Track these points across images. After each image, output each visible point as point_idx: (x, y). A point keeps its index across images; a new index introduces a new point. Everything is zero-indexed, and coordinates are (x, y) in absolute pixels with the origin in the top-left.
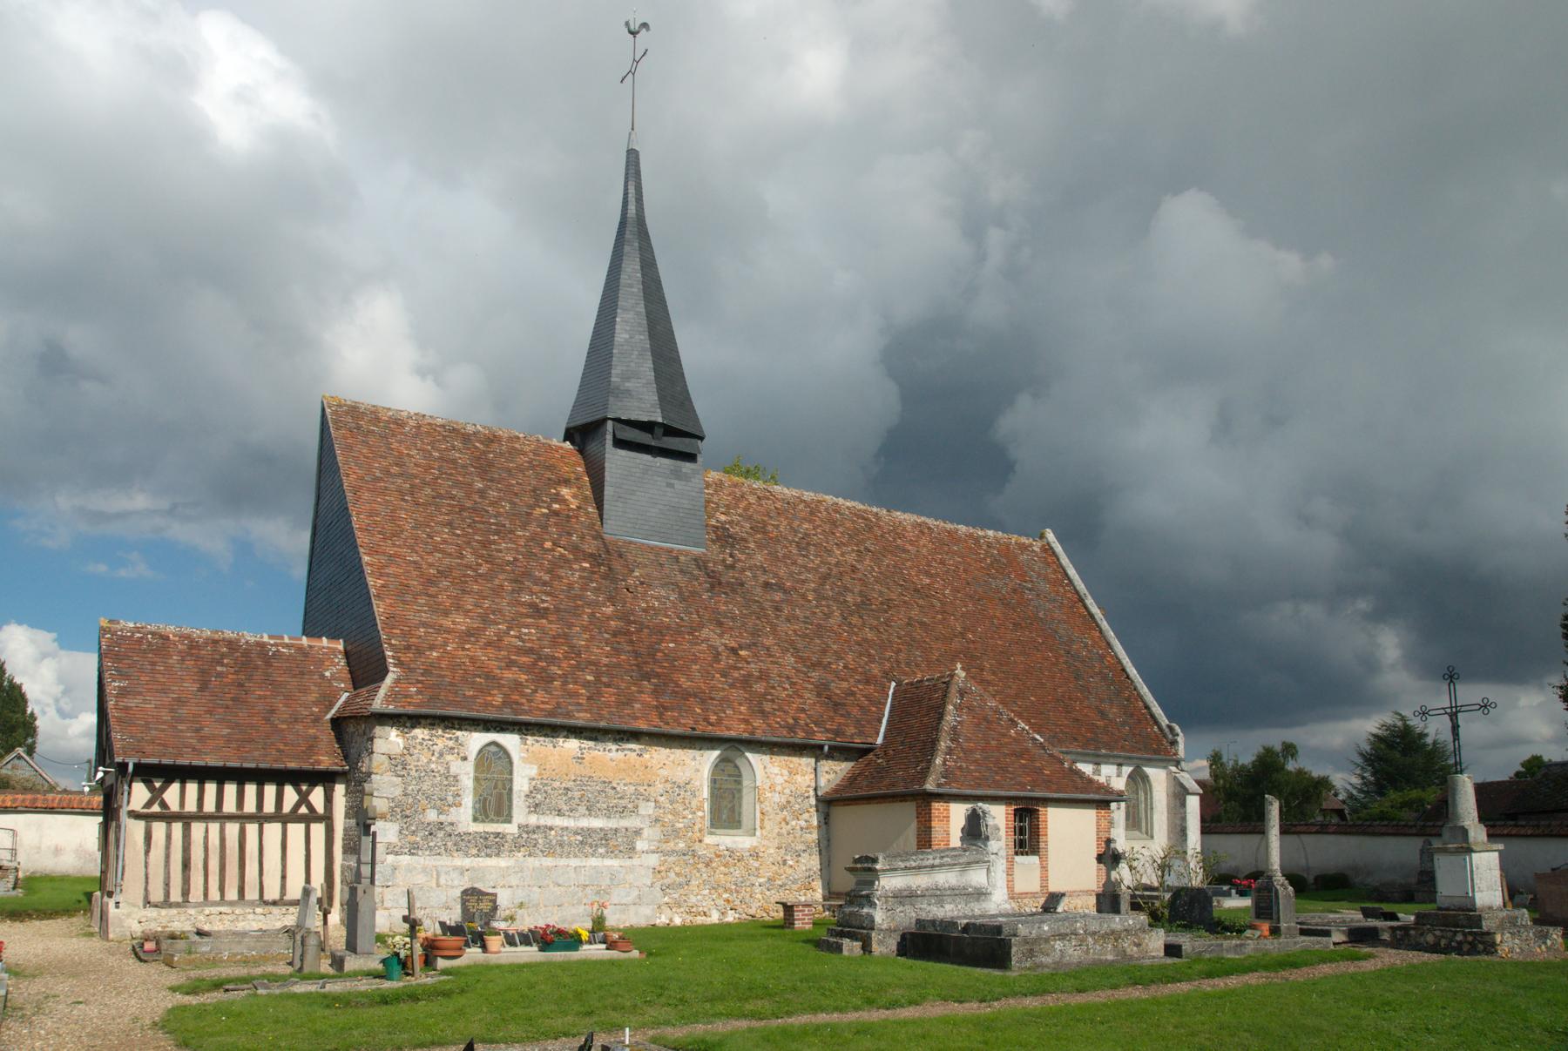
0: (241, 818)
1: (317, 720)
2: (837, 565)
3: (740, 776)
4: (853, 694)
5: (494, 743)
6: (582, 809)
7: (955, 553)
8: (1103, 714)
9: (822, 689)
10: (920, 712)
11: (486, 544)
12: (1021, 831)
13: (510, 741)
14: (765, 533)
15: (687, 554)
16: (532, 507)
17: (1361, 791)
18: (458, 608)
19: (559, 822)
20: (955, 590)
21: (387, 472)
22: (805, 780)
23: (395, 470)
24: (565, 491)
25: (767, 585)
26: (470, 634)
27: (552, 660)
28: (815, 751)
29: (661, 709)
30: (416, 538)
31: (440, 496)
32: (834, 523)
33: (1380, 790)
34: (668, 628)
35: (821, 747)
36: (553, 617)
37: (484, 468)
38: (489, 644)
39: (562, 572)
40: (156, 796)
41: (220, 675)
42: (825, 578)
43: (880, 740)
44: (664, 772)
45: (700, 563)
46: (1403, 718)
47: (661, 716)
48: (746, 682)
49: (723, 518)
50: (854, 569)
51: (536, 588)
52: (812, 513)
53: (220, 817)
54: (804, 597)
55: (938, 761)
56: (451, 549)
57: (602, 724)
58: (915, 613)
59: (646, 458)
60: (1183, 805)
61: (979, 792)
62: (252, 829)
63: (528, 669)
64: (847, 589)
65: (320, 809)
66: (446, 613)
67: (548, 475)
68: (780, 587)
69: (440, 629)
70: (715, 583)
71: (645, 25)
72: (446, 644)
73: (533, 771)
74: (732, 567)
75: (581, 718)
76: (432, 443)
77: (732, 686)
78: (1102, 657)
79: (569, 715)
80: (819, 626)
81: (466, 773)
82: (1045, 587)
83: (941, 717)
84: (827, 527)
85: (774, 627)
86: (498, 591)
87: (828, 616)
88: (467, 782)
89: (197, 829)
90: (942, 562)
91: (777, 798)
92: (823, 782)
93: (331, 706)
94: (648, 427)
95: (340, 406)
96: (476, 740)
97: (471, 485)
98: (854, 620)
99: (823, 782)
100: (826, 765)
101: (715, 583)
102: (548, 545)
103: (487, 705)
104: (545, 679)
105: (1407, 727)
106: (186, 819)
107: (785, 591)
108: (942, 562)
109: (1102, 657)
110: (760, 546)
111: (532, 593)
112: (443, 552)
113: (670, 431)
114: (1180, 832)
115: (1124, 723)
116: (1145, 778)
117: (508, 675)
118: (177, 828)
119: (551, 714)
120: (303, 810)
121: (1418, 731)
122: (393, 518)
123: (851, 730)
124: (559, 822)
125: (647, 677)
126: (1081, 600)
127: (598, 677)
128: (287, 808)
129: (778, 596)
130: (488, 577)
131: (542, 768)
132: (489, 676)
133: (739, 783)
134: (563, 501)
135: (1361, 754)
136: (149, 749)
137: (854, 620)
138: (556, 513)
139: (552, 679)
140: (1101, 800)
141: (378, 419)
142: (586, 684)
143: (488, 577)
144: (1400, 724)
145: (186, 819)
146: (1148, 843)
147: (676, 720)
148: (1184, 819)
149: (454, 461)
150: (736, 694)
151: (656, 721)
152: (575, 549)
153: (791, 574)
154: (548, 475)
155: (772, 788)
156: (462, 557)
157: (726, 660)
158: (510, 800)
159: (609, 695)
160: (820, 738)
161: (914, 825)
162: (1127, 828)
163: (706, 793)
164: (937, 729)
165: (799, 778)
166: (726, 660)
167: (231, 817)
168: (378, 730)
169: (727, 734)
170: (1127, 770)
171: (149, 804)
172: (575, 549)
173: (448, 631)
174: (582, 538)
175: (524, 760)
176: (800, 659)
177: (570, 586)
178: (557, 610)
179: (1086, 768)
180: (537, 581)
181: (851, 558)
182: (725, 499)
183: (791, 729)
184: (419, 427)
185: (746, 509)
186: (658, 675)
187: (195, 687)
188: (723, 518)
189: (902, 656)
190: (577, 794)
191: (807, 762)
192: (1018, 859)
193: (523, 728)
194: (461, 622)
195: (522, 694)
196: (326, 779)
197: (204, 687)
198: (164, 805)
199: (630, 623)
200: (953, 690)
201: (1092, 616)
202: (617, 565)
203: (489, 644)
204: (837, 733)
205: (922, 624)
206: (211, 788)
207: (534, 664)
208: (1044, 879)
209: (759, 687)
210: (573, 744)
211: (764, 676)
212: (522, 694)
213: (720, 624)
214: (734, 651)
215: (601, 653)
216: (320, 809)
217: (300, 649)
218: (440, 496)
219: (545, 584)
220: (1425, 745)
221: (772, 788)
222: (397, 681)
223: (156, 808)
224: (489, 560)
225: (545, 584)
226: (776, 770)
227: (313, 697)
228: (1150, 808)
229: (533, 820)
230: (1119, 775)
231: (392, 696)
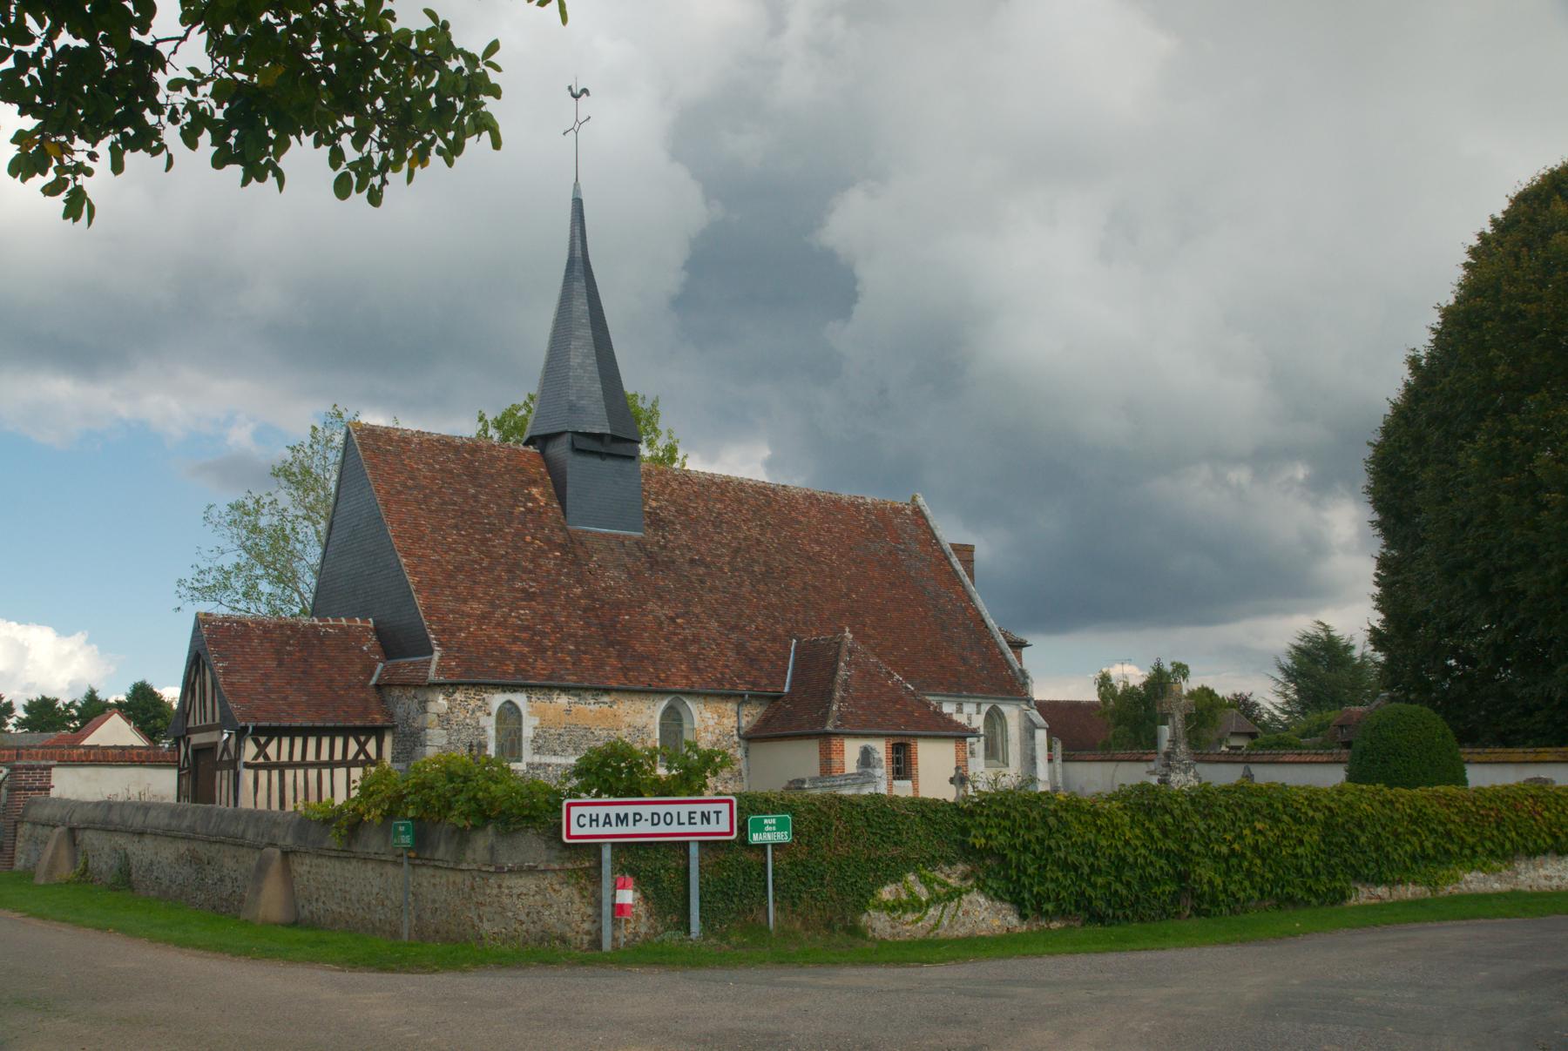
0: (319, 765)
1: (364, 686)
2: (745, 539)
3: (681, 720)
4: (764, 651)
5: (509, 702)
6: (570, 750)
7: (840, 521)
8: (964, 660)
9: (740, 648)
10: (817, 665)
11: (484, 541)
12: (898, 761)
13: (520, 699)
14: (687, 515)
15: (630, 538)
16: (513, 506)
17: (1283, 711)
18: (474, 597)
19: (554, 760)
20: (841, 556)
21: (404, 485)
22: (730, 722)
23: (410, 483)
24: (534, 491)
25: (692, 561)
26: (484, 617)
27: (543, 634)
28: (740, 699)
29: (625, 671)
30: (435, 540)
31: (445, 503)
32: (740, 501)
33: (49, 768)
34: (623, 603)
35: (742, 696)
36: (540, 600)
37: (474, 476)
38: (499, 624)
39: (542, 561)
40: (262, 749)
41: (289, 653)
42: (737, 551)
43: (786, 689)
44: (627, 719)
45: (640, 544)
46: (1326, 629)
47: (625, 675)
48: (683, 644)
49: (654, 504)
50: (758, 542)
51: (525, 576)
52: (722, 494)
53: (304, 764)
54: (721, 569)
55: (835, 708)
56: (460, 548)
57: (586, 684)
58: (809, 578)
59: (596, 461)
60: (1033, 737)
61: (866, 731)
62: (326, 773)
63: (528, 643)
64: (754, 561)
65: (373, 755)
66: (465, 601)
67: (521, 477)
68: (702, 562)
69: (463, 614)
70: (654, 562)
71: (585, 91)
72: (468, 627)
73: (536, 722)
74: (665, 547)
75: (571, 680)
76: (432, 457)
77: (674, 649)
78: (965, 609)
79: (561, 678)
80: (734, 594)
81: (490, 724)
82: (916, 547)
83: (835, 672)
84: (735, 506)
85: (701, 598)
86: (498, 580)
87: (740, 585)
88: (491, 732)
89: (289, 774)
90: (829, 530)
91: (709, 737)
92: (743, 723)
93: (372, 674)
94: (599, 437)
95: (362, 430)
96: (497, 700)
97: (466, 491)
98: (761, 587)
99: (743, 723)
100: (745, 710)
101: (654, 562)
102: (528, 538)
103: (505, 673)
104: (540, 650)
105: (1330, 637)
106: (281, 767)
107: (707, 567)
108: (829, 530)
109: (965, 609)
110: (685, 527)
111: (522, 580)
112: (454, 550)
113: (616, 439)
114: (1031, 761)
115: (983, 668)
116: (1001, 715)
117: (515, 648)
118: (275, 774)
119: (550, 678)
120: (362, 757)
121: (1343, 642)
122: (417, 526)
123: (765, 681)
124: (554, 760)
125: (612, 644)
126: (947, 558)
127: (577, 644)
128: (350, 756)
129: (702, 570)
130: (490, 569)
131: (543, 720)
132: (502, 650)
133: (681, 725)
134: (534, 500)
135: (1282, 669)
136: (258, 715)
137: (761, 587)
138: (530, 511)
139: (544, 650)
140: (960, 735)
141: (391, 439)
142: (570, 653)
143: (490, 569)
144: (1323, 634)
145: (281, 767)
146: (1005, 771)
147: (637, 678)
148: (1033, 749)
149: (451, 472)
150: (678, 655)
151: (623, 680)
152: (548, 541)
153: (710, 550)
154: (521, 477)
155: (706, 729)
156: (469, 554)
157: (668, 628)
158: (520, 744)
159: (587, 660)
160: (742, 688)
161: (817, 756)
162: (987, 757)
163: (657, 735)
164: (832, 681)
165: (725, 721)
166: (668, 628)
167: (312, 765)
168: (430, 696)
169: (674, 688)
170: (985, 708)
171: (256, 757)
172: (548, 541)
173: (469, 616)
174: (552, 531)
175: (530, 714)
176: (722, 624)
177: (548, 572)
178: (542, 593)
179: (948, 708)
180: (525, 570)
181: (755, 532)
182: (655, 487)
183: (720, 682)
184: (421, 444)
185: (671, 495)
186: (619, 643)
187: (275, 664)
188: (654, 504)
189: (800, 617)
190: (566, 739)
191: (730, 706)
192: (896, 783)
193: (527, 688)
194: (476, 607)
195: (528, 664)
196: (378, 732)
197: (280, 663)
198: (266, 757)
199: (595, 600)
200: (843, 650)
201: (956, 572)
202: (580, 553)
203: (499, 624)
204: (754, 684)
205: (815, 587)
206: (286, 742)
207: (532, 638)
208: (916, 789)
209: (693, 649)
210: (563, 700)
211: (696, 639)
212: (528, 664)
213: (660, 598)
214: (672, 620)
215: (577, 626)
216: (373, 755)
217: (342, 628)
218: (445, 503)
219: (531, 572)
220: (1352, 659)
221: (706, 729)
222: (441, 658)
223: (261, 760)
224: (489, 555)
225: (531, 572)
226: (709, 715)
227: (358, 668)
228: (1006, 740)
229: (537, 759)
230: (978, 713)
231: (440, 671)
